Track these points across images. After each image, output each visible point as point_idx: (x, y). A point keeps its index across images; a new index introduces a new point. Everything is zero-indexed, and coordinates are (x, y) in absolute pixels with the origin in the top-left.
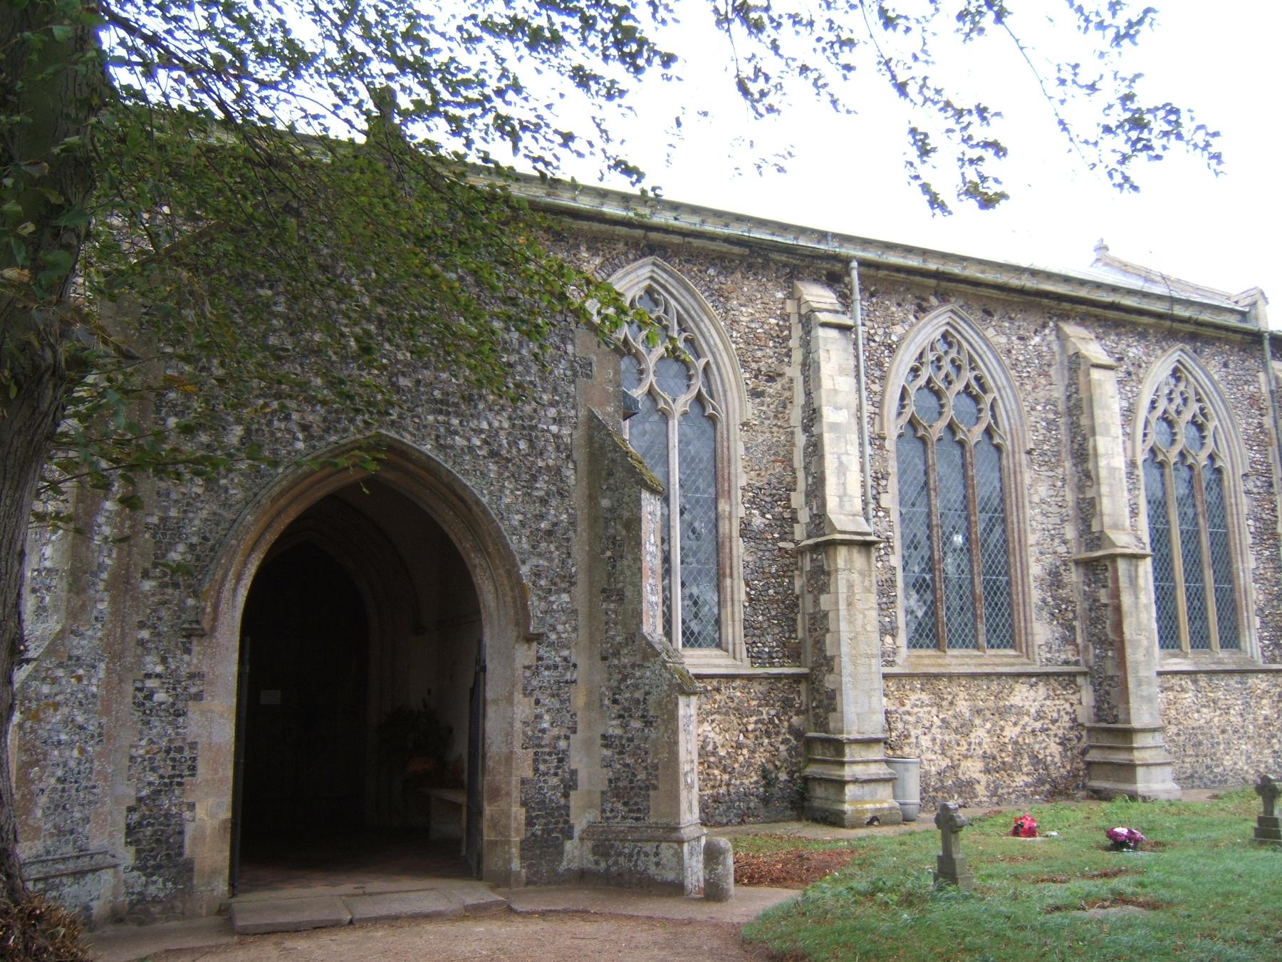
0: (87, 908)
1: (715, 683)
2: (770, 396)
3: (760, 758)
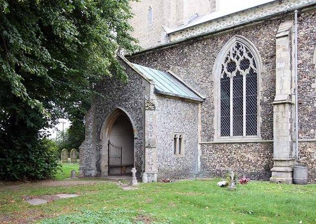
0: (91, 174)
1: (252, 144)
2: (271, 62)
3: (264, 164)
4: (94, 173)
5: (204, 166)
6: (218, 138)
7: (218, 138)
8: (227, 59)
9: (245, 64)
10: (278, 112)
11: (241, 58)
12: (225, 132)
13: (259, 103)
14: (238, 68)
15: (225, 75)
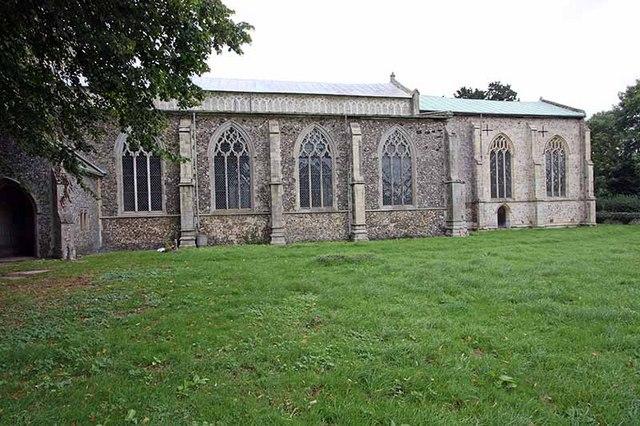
4: (50, 253)
5: (106, 240)
6: (121, 212)
7: (121, 212)
8: (221, 139)
9: (238, 147)
10: (183, 192)
11: (235, 142)
12: (129, 206)
13: (163, 183)
14: (232, 149)
15: (128, 153)
